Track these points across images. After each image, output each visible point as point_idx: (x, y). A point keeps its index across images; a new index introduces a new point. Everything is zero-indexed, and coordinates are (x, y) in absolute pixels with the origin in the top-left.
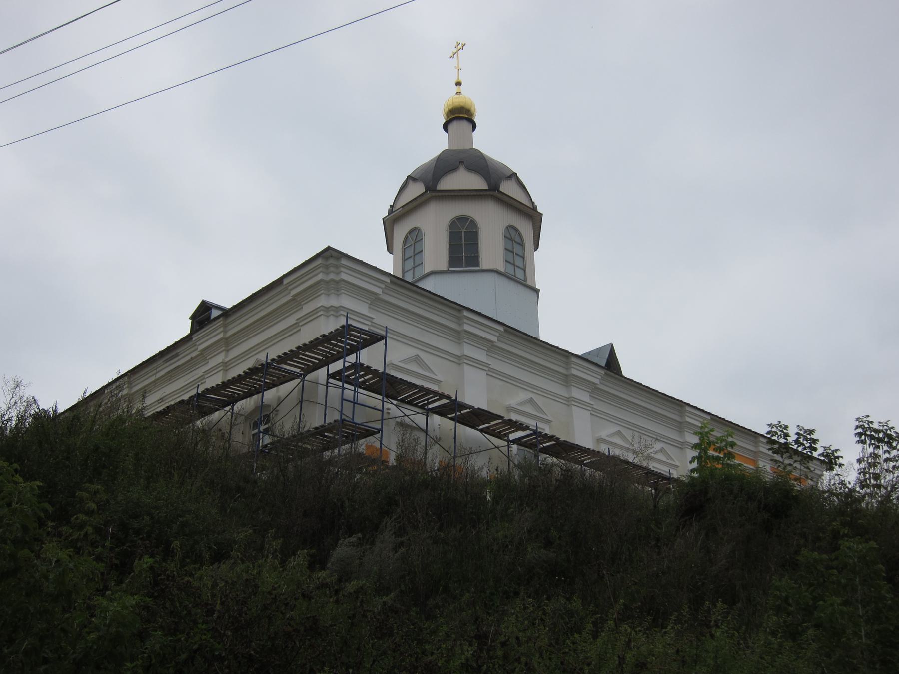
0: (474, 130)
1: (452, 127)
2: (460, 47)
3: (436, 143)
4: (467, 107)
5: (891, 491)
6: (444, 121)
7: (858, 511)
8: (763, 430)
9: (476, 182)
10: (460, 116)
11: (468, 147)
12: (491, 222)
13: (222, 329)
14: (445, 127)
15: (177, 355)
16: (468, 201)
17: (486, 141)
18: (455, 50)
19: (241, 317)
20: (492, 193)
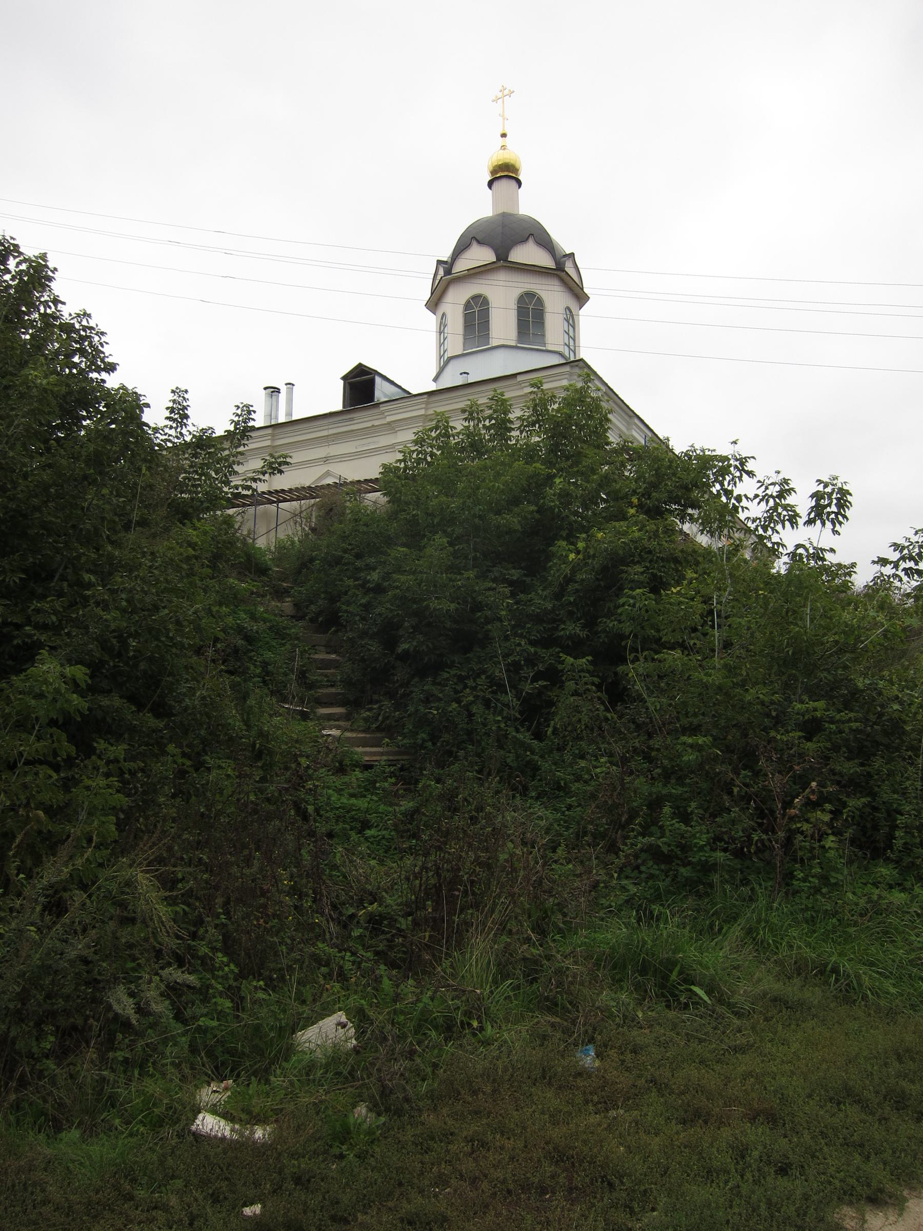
0: (520, 187)
1: (496, 185)
2: (506, 92)
3: (481, 206)
4: (517, 166)
5: (67, 861)
6: (489, 178)
7: (670, 565)
8: (661, 438)
9: (544, 259)
10: (505, 174)
11: (515, 213)
12: (554, 298)
13: (424, 406)
14: (490, 184)
15: (352, 419)
16: (509, 261)
17: (529, 204)
18: (500, 95)
19: (447, 399)
20: (558, 273)
